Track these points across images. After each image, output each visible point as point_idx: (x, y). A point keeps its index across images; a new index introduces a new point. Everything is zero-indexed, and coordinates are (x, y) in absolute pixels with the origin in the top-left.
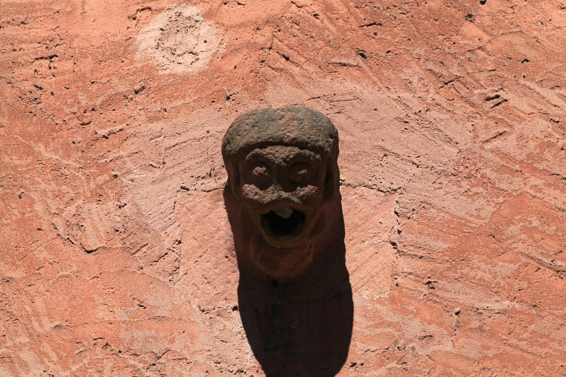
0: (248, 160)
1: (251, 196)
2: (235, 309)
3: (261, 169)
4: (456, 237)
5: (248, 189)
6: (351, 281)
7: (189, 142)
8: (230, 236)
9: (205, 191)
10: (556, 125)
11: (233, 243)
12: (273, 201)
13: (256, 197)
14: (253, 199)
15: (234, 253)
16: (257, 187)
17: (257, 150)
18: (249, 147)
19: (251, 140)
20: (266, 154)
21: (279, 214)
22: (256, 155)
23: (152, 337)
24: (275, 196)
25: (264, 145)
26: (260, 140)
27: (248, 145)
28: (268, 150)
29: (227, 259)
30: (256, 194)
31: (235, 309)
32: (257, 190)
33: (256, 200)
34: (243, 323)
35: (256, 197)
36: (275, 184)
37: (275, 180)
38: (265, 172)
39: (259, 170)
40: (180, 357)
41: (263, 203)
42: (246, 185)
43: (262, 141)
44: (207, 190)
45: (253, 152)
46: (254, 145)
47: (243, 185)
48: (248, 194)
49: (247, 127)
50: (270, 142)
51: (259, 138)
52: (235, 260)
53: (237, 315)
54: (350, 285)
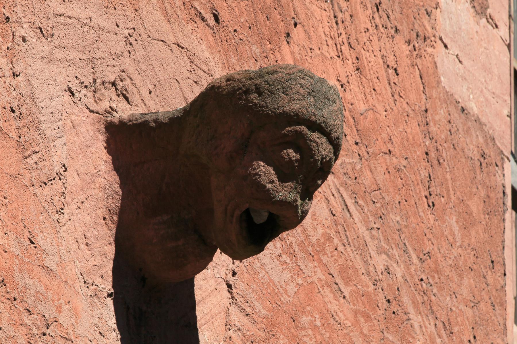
0: (285, 133)
1: (264, 180)
2: (109, 295)
3: (294, 154)
4: (271, 305)
5: (262, 168)
6: (197, 313)
7: (73, 20)
8: (117, 193)
9: (88, 108)
10: (332, 217)
11: (119, 205)
12: (286, 201)
13: (270, 186)
14: (265, 186)
15: (116, 218)
16: (276, 174)
17: (304, 128)
18: (296, 119)
19: (304, 111)
20: (310, 140)
21: (252, 214)
22: (300, 134)
23: (41, 294)
24: (290, 197)
25: (315, 126)
26: (314, 118)
27: (297, 115)
28: (315, 136)
29: (104, 222)
30: (272, 182)
31: (109, 295)
32: (275, 177)
33: (268, 190)
34: (117, 319)
35: (270, 186)
36: (297, 183)
37: (301, 177)
38: (297, 161)
39: (292, 154)
40: (67, 336)
41: (273, 198)
42: (262, 163)
43: (316, 122)
44: (91, 109)
45: (297, 128)
46: (304, 119)
47: (257, 160)
48: (260, 175)
49: (302, 91)
50: (322, 127)
51: (314, 115)
52: (114, 227)
53: (110, 302)
54: (195, 317)
